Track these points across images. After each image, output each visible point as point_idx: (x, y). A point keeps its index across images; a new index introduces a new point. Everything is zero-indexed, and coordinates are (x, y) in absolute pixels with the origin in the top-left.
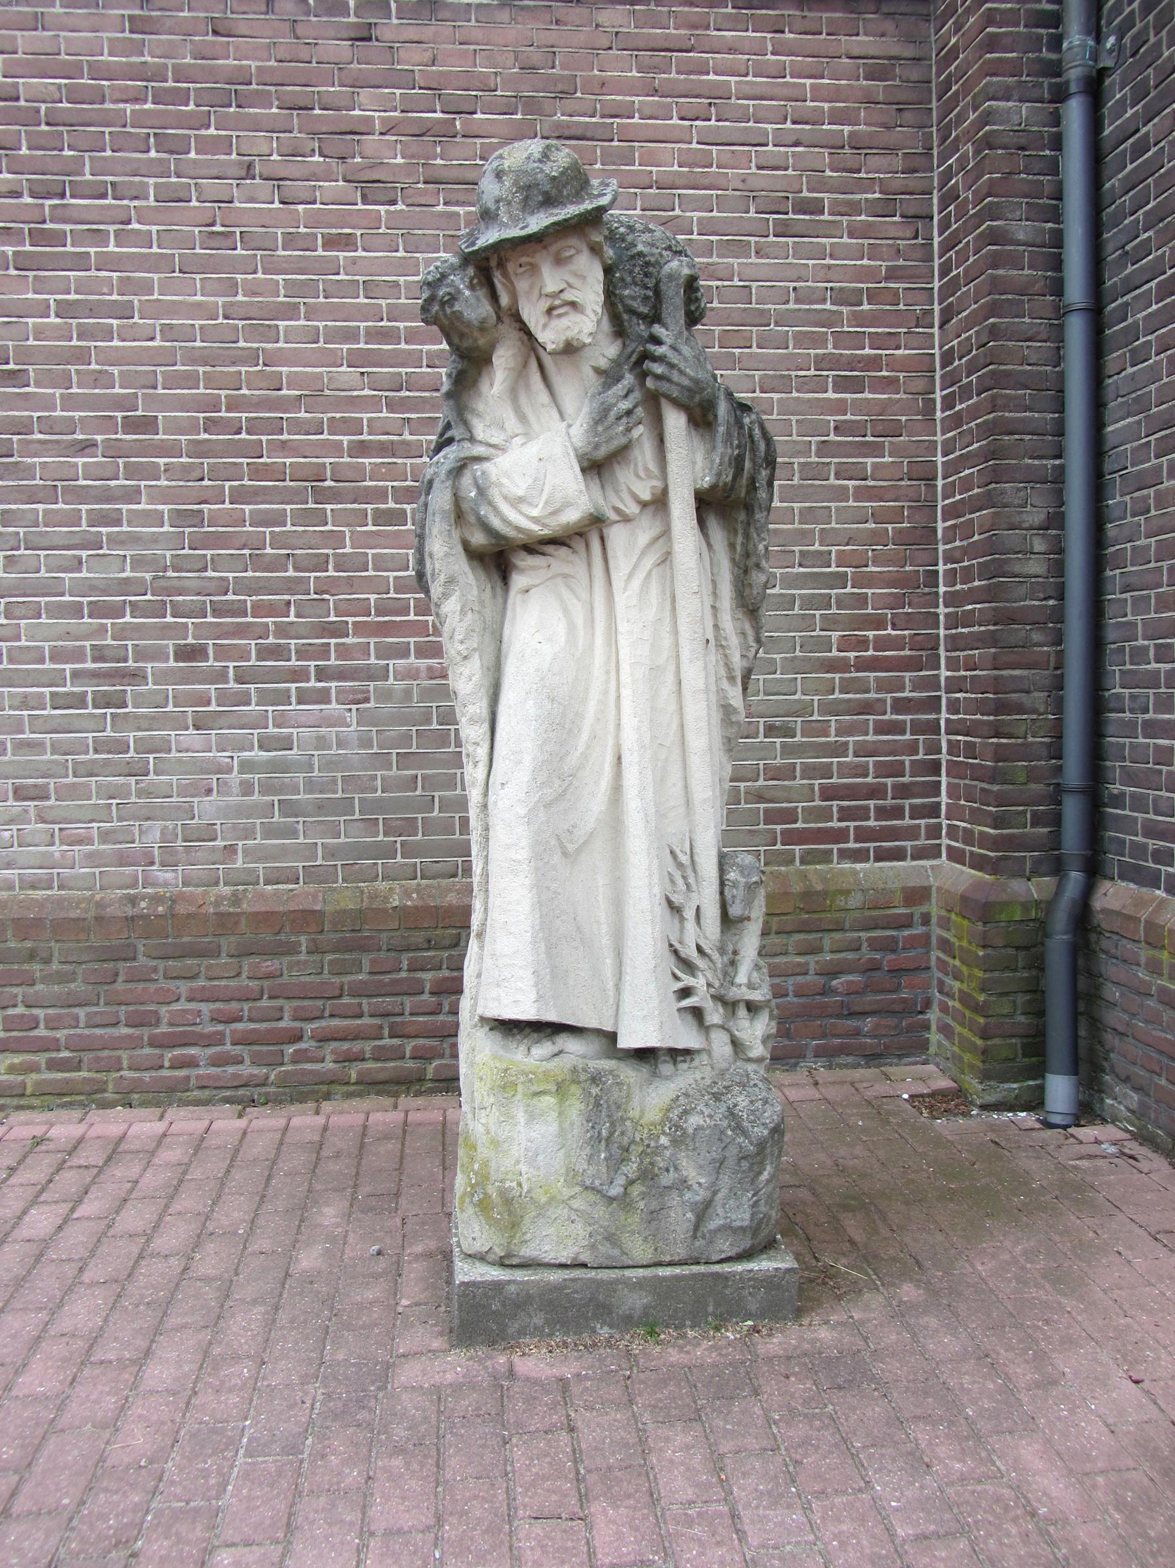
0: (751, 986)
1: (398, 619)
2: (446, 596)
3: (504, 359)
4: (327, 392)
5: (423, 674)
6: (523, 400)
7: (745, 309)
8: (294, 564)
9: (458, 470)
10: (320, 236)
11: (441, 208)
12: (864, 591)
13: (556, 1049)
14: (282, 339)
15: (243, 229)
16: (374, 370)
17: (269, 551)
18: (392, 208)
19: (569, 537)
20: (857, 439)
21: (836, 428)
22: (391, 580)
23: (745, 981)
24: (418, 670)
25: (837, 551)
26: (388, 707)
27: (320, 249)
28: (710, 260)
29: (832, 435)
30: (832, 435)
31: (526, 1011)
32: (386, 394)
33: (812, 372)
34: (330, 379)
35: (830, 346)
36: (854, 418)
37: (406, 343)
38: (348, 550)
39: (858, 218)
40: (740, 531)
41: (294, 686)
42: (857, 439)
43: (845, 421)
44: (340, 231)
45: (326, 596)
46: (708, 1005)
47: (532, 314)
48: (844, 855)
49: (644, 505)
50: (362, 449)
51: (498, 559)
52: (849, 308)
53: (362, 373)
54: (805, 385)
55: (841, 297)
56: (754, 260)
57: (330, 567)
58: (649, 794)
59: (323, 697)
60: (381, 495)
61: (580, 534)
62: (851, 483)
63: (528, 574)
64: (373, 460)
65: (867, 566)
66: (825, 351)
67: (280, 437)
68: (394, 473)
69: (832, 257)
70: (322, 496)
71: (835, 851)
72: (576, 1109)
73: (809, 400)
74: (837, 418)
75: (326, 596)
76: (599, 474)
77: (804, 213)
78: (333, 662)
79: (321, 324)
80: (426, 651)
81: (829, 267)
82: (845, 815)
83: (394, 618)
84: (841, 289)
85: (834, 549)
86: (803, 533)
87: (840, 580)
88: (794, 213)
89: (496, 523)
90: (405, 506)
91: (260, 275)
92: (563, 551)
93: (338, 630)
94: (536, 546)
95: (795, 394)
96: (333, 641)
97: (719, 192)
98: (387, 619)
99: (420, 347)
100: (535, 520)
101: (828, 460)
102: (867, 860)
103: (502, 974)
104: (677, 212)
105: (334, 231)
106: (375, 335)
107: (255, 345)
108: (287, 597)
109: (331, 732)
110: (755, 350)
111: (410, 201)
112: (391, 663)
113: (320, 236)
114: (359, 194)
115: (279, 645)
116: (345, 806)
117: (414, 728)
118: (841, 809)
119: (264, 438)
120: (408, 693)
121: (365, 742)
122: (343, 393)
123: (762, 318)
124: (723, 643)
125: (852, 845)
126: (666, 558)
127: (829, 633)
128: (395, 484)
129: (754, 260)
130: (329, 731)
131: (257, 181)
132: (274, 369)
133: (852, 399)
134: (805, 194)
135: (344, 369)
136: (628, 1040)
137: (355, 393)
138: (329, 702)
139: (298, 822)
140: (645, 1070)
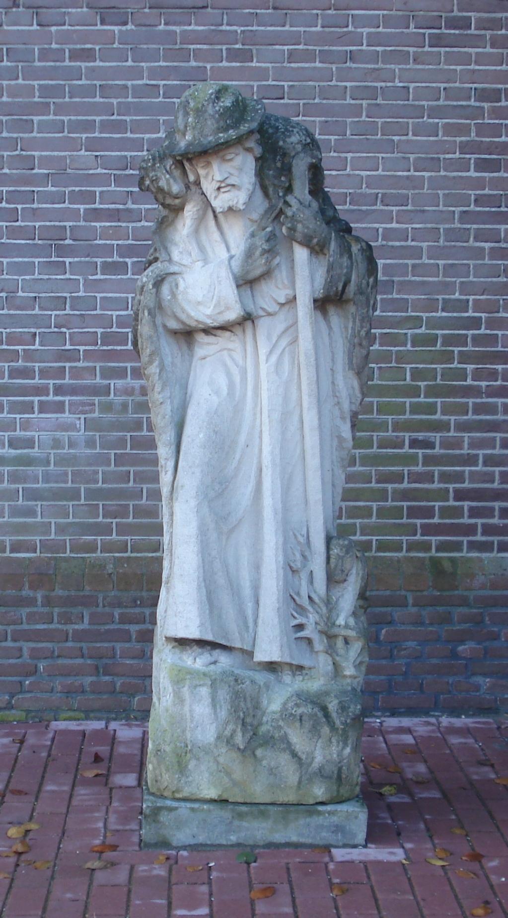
0: (347, 626)
1: (119, 348)
2: (151, 362)
3: (190, 211)
4: (69, 171)
5: (137, 392)
6: (203, 238)
7: (405, 105)
8: (39, 305)
9: (158, 283)
10: (67, 51)
11: (162, 27)
12: (495, 332)
13: (213, 660)
14: (35, 129)
15: (9, 46)
16: (106, 153)
17: (20, 294)
18: (124, 28)
19: (232, 326)
20: (493, 209)
21: (476, 201)
22: (114, 317)
23: (343, 623)
24: (133, 388)
25: (474, 300)
26: (109, 417)
27: (67, 60)
28: (376, 66)
29: (472, 206)
30: (472, 206)
31: (193, 632)
32: (115, 172)
33: (457, 155)
34: (71, 161)
35: (473, 134)
36: (491, 192)
37: (131, 132)
38: (81, 294)
39: (499, 32)
40: (351, 320)
41: (36, 399)
42: (493, 209)
43: (484, 195)
44: (83, 46)
45: (64, 330)
46: (316, 637)
47: (208, 187)
48: (473, 546)
49: (282, 305)
50: (96, 214)
51: (187, 335)
52: (489, 104)
53: (96, 156)
54: (451, 165)
55: (483, 95)
56: (411, 66)
57: (67, 307)
58: (278, 496)
59: (59, 408)
60: (109, 250)
61: (239, 324)
62: (487, 245)
63: (206, 347)
64: (103, 224)
65: (498, 312)
66: (468, 139)
67: (32, 206)
68: (117, 233)
69: (477, 63)
70: (62, 251)
71: (465, 543)
72: (223, 694)
73: (454, 177)
74: (478, 192)
75: (64, 330)
76: (251, 288)
77: (454, 29)
78: (67, 381)
79: (66, 119)
80: (137, 373)
81: (474, 71)
82: (474, 513)
83: (115, 348)
84: (483, 90)
85: (471, 298)
86: (446, 285)
87: (475, 323)
88: (446, 28)
89: (183, 317)
90: (127, 260)
91: (20, 81)
92: (228, 334)
93: (70, 356)
94: (208, 331)
95: (442, 173)
96: (67, 365)
97: (385, 12)
98: (110, 348)
99: (141, 136)
100: (209, 317)
101: (469, 226)
102: (492, 550)
103: (179, 610)
104: (350, 28)
105: (78, 46)
106: (106, 126)
107: (15, 135)
108: (33, 330)
109: (64, 436)
110: (410, 137)
111: (138, 22)
112: (112, 382)
113: (67, 51)
114: (98, 17)
115: (26, 367)
116: (74, 495)
117: (129, 434)
118: (471, 509)
119: (19, 207)
120: (125, 406)
121: (90, 443)
122: (81, 172)
123: (419, 112)
124: (337, 394)
125: (479, 538)
126: (295, 341)
127: (465, 366)
128: (120, 242)
129: (411, 66)
130: (59, 432)
131: (21, 9)
132: (29, 153)
133: (490, 178)
134: (456, 13)
135: (83, 152)
136: (261, 656)
137: (91, 172)
138: (63, 412)
139: (37, 505)
140: (271, 677)
